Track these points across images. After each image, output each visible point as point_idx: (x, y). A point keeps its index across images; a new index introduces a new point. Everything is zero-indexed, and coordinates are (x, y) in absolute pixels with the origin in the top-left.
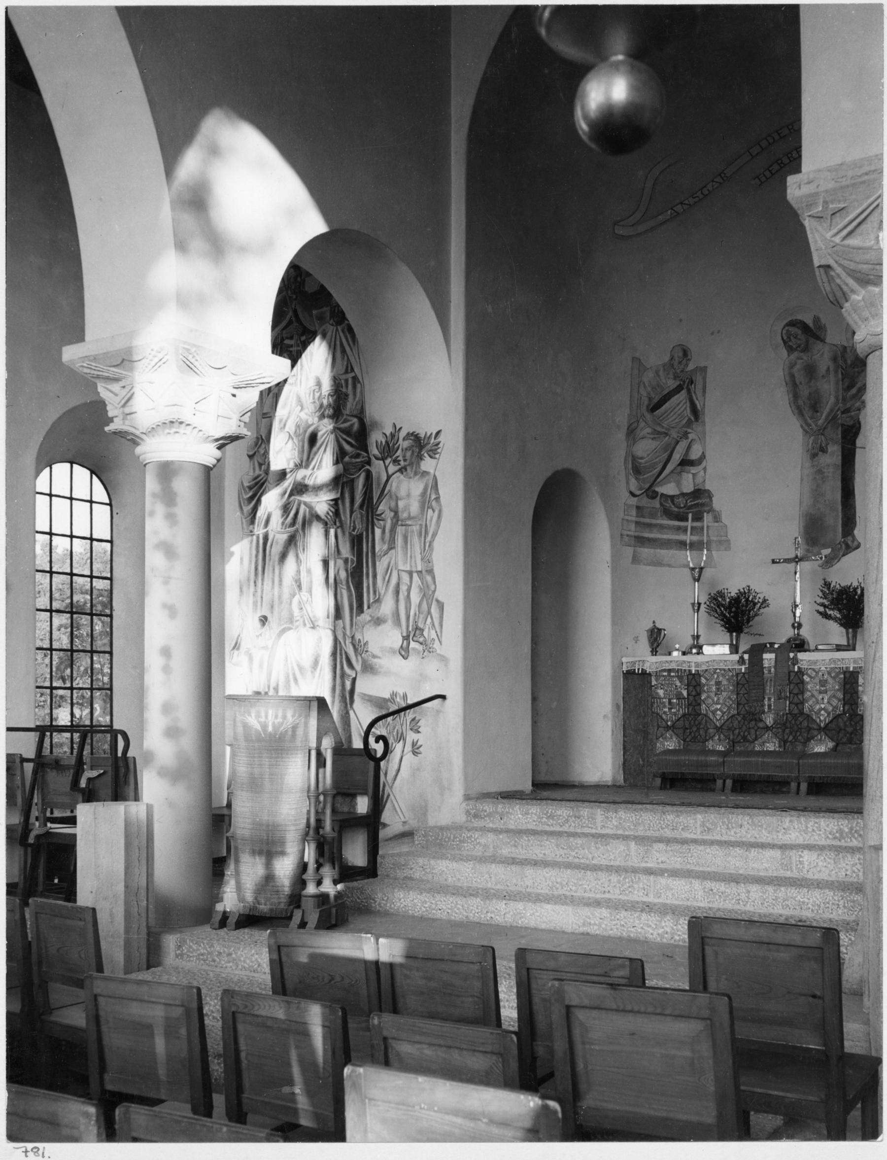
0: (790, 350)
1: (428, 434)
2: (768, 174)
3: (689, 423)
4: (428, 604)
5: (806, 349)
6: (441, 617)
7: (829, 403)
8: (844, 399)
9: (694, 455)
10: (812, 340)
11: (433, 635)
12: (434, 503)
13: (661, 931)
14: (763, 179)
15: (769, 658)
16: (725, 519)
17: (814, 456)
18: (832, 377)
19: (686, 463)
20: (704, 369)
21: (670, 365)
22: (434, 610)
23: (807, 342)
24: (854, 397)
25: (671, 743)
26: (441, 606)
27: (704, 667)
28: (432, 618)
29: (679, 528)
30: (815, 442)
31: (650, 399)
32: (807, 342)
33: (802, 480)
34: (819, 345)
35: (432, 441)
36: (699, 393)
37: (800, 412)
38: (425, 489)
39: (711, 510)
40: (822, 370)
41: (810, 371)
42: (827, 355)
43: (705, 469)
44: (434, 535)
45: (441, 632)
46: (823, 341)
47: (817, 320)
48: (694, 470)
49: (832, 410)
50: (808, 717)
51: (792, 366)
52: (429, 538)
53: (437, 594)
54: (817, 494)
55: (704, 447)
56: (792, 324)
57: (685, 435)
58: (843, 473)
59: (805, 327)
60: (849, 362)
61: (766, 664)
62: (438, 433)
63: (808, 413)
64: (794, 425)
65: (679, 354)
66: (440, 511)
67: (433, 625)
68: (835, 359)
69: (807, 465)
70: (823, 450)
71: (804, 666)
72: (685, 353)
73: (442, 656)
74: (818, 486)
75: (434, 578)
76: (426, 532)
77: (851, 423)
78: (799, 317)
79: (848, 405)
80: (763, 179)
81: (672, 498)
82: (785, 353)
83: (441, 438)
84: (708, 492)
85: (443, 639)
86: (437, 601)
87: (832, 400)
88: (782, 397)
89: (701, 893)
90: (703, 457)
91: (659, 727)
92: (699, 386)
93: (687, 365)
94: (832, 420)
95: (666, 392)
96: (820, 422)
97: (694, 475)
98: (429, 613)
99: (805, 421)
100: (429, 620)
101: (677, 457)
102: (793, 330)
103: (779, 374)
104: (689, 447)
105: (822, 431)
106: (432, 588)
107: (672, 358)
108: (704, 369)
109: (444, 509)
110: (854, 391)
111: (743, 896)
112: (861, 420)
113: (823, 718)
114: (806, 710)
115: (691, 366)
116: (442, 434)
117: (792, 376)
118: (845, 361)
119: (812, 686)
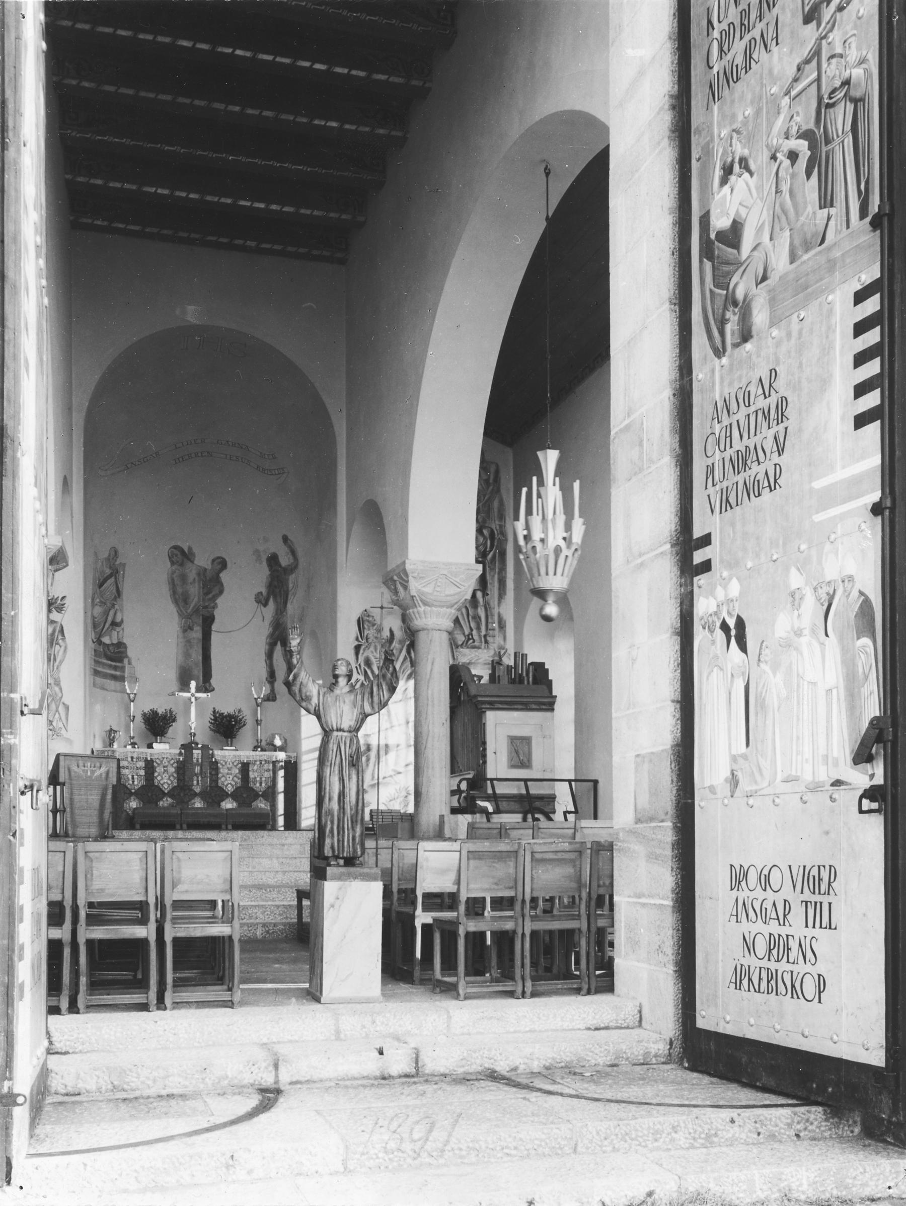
0: (173, 563)
1: (56, 597)
2: (181, 460)
3: (115, 599)
4: (56, 705)
5: (182, 565)
6: (67, 714)
7: (194, 600)
8: (204, 600)
9: (118, 620)
10: (185, 560)
11: (61, 725)
12: (60, 641)
13: (276, 880)
14: (177, 461)
15: (197, 753)
16: (133, 663)
17: (185, 631)
18: (196, 585)
19: (114, 624)
20: (124, 565)
21: (108, 559)
22: (61, 709)
23: (183, 561)
24: (210, 600)
25: (134, 804)
26: (67, 708)
27: (156, 757)
28: (59, 714)
29: (115, 668)
30: (186, 622)
31: (99, 580)
32: (183, 561)
33: (178, 645)
34: (189, 564)
35: (59, 602)
36: (121, 580)
37: (176, 602)
38: (54, 631)
39: (127, 657)
40: (191, 579)
41: (183, 578)
42: (194, 572)
43: (123, 629)
44: (61, 662)
45: (67, 723)
46: (192, 562)
47: (190, 548)
48: (118, 629)
49: (196, 605)
50: (221, 788)
51: (173, 573)
52: (57, 664)
53: (63, 700)
54: (187, 655)
55: (122, 615)
56: (175, 547)
57: (113, 605)
58: (203, 645)
59: (182, 551)
60: (208, 578)
61: (195, 756)
62: (63, 598)
63: (181, 604)
64: (172, 609)
65: (113, 553)
66: (66, 648)
67: (60, 719)
68: (199, 574)
69: (181, 635)
70: (191, 628)
71: (218, 758)
72: (116, 552)
73: (68, 739)
74: (187, 650)
75: (61, 689)
76: (55, 659)
77: (208, 615)
78: (179, 544)
79: (207, 604)
80: (177, 461)
81: (108, 645)
82: (169, 564)
83: (66, 601)
84: (124, 644)
85: (69, 729)
86: (64, 704)
87: (196, 599)
88: (166, 590)
89: (277, 865)
90: (122, 621)
91: (125, 793)
92: (121, 576)
93: (116, 561)
94: (196, 611)
95: (105, 576)
96: (189, 611)
97: (118, 632)
98: (57, 711)
99: (179, 608)
100: (57, 715)
101: (110, 619)
102: (176, 552)
103: (164, 578)
104: (115, 614)
105: (189, 617)
106: (60, 695)
107: (109, 555)
108: (124, 565)
109: (69, 647)
110: (210, 596)
111: (298, 864)
112: (217, 613)
113: (230, 789)
114: (220, 784)
115: (117, 563)
116: (67, 598)
117: (173, 580)
118: (205, 577)
119: (223, 771)
